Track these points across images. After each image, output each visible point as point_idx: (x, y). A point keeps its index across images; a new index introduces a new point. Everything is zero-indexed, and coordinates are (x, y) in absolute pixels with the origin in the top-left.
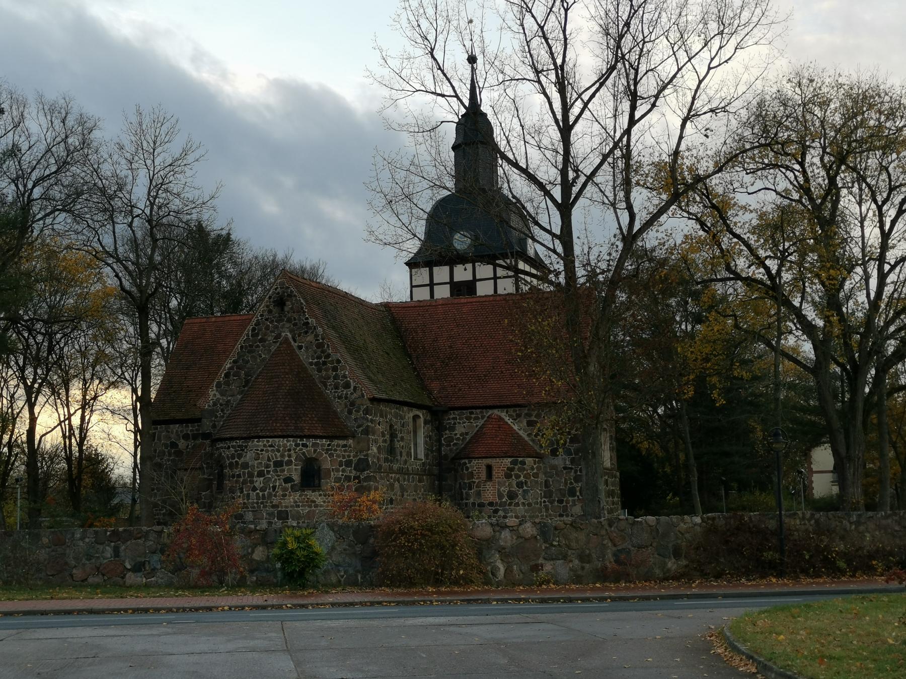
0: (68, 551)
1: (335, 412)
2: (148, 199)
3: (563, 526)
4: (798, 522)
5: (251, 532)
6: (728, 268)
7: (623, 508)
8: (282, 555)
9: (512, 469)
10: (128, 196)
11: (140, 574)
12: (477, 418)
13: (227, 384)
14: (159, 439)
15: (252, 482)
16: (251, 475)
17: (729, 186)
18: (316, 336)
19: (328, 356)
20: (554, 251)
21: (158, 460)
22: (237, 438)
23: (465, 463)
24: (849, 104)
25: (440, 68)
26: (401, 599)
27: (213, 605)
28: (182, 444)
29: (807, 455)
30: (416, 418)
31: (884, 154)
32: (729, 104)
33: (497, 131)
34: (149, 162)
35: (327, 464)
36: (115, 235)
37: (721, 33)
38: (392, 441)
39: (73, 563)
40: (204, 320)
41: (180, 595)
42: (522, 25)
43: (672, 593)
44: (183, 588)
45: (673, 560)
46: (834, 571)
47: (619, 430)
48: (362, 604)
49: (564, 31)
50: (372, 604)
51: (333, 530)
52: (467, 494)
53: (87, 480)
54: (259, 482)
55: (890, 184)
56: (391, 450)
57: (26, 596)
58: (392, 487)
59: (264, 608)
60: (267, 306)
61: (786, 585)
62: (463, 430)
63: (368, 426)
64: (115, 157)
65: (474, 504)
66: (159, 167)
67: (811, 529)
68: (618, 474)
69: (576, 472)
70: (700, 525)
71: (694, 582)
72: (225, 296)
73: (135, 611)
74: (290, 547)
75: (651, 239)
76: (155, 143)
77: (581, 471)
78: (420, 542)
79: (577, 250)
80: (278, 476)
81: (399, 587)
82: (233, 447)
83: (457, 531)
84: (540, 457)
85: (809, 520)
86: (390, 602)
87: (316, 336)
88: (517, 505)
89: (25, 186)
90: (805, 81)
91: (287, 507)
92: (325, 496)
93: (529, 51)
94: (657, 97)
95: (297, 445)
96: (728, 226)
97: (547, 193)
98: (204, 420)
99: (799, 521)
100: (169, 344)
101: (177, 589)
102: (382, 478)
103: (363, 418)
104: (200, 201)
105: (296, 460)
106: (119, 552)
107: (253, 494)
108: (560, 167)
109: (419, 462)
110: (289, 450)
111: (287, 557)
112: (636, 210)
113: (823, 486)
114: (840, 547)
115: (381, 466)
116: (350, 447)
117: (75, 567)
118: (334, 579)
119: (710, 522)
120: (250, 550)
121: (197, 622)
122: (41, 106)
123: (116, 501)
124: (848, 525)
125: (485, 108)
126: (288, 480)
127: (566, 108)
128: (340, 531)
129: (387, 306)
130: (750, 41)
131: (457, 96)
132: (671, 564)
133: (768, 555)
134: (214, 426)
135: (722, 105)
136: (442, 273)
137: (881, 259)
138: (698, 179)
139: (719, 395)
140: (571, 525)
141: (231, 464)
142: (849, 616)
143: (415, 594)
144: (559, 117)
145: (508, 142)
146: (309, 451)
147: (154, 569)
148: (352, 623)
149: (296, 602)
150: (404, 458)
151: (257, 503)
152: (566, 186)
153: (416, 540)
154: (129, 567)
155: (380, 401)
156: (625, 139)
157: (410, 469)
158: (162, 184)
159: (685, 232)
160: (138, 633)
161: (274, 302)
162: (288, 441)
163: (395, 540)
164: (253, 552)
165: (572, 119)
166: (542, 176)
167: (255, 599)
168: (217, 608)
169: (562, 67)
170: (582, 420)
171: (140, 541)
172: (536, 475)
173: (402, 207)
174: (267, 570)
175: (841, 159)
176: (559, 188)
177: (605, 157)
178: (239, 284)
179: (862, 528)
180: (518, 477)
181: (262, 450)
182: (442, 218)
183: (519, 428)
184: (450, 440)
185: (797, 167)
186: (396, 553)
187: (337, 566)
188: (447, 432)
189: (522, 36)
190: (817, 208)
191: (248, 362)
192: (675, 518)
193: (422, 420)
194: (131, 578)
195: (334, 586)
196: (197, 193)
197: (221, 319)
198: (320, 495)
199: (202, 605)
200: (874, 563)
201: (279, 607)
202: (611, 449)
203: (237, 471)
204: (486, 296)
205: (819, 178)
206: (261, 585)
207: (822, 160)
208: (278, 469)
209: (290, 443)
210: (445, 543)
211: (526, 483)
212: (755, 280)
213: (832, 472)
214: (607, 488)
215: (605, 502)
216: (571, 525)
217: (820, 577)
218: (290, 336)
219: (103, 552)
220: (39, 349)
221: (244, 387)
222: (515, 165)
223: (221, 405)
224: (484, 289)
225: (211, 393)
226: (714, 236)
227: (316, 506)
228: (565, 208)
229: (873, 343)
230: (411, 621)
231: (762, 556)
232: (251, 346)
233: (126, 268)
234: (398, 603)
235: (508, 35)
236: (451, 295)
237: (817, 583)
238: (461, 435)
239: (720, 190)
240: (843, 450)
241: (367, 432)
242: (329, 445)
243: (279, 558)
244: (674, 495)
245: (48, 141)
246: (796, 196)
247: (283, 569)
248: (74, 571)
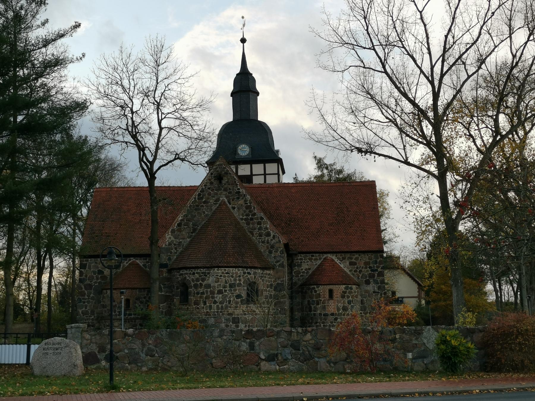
1: (260, 251)
11: (272, 363)
12: (316, 259)
13: (180, 230)
14: (90, 268)
16: (212, 293)
21: (88, 282)
22: (201, 268)
23: (314, 288)
28: (107, 272)
35: (261, 287)
39: (213, 354)
62: (307, 267)
65: (320, 314)
80: (232, 293)
82: (197, 273)
91: (238, 315)
103: (280, 256)
105: (244, 283)
106: (254, 346)
107: (214, 306)
110: (240, 276)
134: (170, 259)
151: (217, 312)
154: (263, 357)
161: (214, 177)
162: (239, 270)
180: (348, 297)
181: (221, 276)
183: (345, 266)
188: (296, 267)
194: (265, 366)
203: (201, 290)
208: (232, 289)
209: (240, 271)
218: (226, 200)
221: (192, 233)
224: (257, 180)
232: (197, 206)
238: (306, 269)
242: (262, 273)
248: (214, 361)
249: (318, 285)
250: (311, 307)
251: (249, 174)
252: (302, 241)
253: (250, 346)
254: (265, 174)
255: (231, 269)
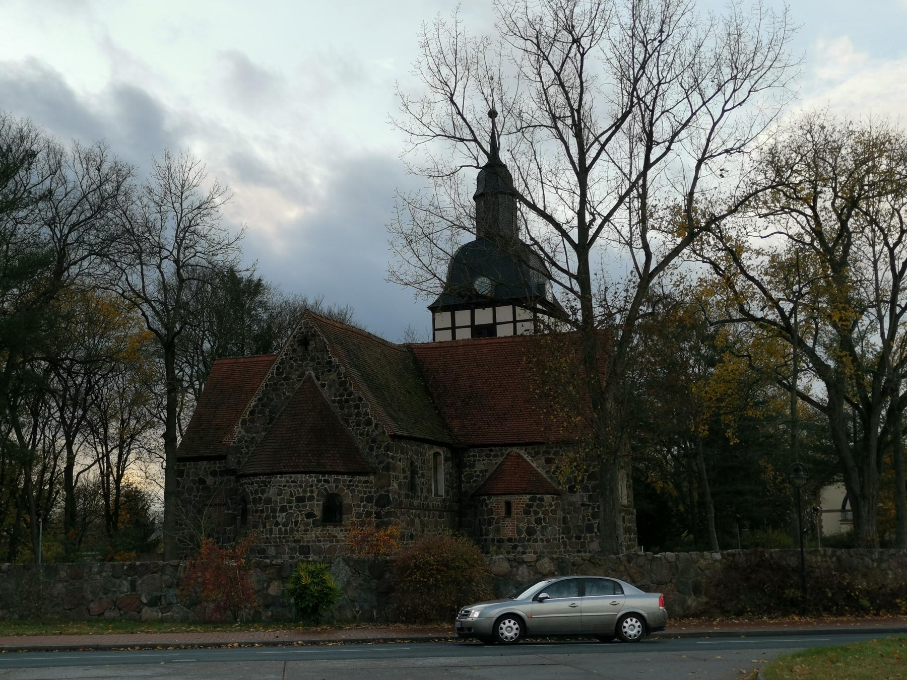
0: (85, 586)
2: (176, 241)
3: (581, 562)
4: (819, 559)
5: (266, 566)
6: (742, 310)
7: (640, 544)
8: (295, 590)
9: (531, 506)
10: (157, 239)
11: (155, 609)
12: (496, 456)
13: (252, 421)
14: (188, 476)
15: (274, 517)
16: (274, 510)
17: (743, 230)
18: (339, 374)
19: (351, 394)
20: (571, 290)
21: (186, 495)
23: (485, 500)
24: (860, 150)
25: (459, 113)
26: (415, 636)
27: (222, 641)
28: (210, 480)
29: (816, 494)
30: (436, 455)
31: (896, 196)
32: (743, 145)
33: (515, 175)
34: (177, 205)
35: (348, 500)
36: (150, 278)
37: (734, 78)
38: (412, 478)
39: (90, 596)
40: (233, 361)
41: (191, 631)
42: (539, 74)
43: (693, 631)
44: (195, 623)
45: (693, 597)
46: (858, 610)
47: (636, 469)
48: (375, 641)
49: (580, 76)
50: (385, 641)
51: (349, 566)
52: (487, 530)
53: (124, 516)
54: (281, 517)
55: (901, 227)
56: (412, 487)
57: (36, 631)
58: (412, 522)
59: (274, 644)
60: (292, 346)
61: (809, 623)
62: (483, 468)
63: (389, 463)
64: (145, 200)
65: (493, 540)
66: (187, 210)
67: (832, 566)
68: (635, 511)
69: (593, 508)
70: (720, 562)
71: (715, 620)
72: (256, 339)
73: (143, 647)
74: (304, 582)
75: (665, 283)
76: (183, 187)
77: (598, 507)
78: (436, 578)
79: (594, 289)
80: (300, 511)
81: (414, 623)
82: (256, 482)
83: (474, 566)
84: (558, 494)
85: (831, 557)
86: (404, 639)
87: (339, 374)
88: (536, 541)
89: (61, 231)
90: (817, 127)
91: (308, 542)
92: (346, 531)
93: (547, 99)
94: (671, 141)
95: (319, 481)
96: (742, 268)
97: (564, 234)
98: (230, 457)
99: (819, 560)
100: (200, 385)
101: (190, 624)
102: (402, 514)
104: (226, 242)
107: (276, 529)
108: (577, 209)
109: (439, 499)
110: (312, 486)
111: (301, 593)
112: (652, 250)
113: (832, 524)
114: (862, 584)
115: (401, 502)
116: (371, 483)
117: (92, 601)
118: (349, 614)
119: (731, 558)
120: (265, 585)
121: (199, 661)
122: (77, 155)
123: (153, 537)
124: (870, 561)
125: (504, 157)
126: (310, 515)
127: (582, 153)
128: (356, 566)
129: (410, 349)
130: (762, 84)
131: (475, 140)
132: (691, 601)
133: (790, 593)
135: (738, 145)
136: (463, 317)
137: (893, 302)
138: (715, 219)
139: (733, 434)
140: (590, 560)
141: (254, 499)
142: (892, 661)
143: (430, 630)
144: (576, 160)
145: (526, 186)
146: (331, 487)
147: (170, 604)
148: (359, 663)
149: (307, 638)
150: (424, 495)
151: (280, 538)
152: (583, 228)
153: (431, 575)
154: (145, 601)
155: (400, 438)
156: (641, 182)
157: (431, 505)
158: (189, 227)
159: (699, 275)
160: (130, 674)
161: (298, 341)
163: (410, 575)
164: (268, 586)
165: (588, 162)
166: (560, 218)
167: (267, 636)
168: (226, 644)
169: (578, 111)
170: (599, 456)
171: (157, 576)
172: (554, 512)
173: (422, 248)
174: (283, 606)
175: (853, 203)
176: (576, 230)
177: (621, 199)
178: (269, 328)
179: (884, 566)
180: (536, 513)
181: (285, 486)
182: (464, 263)
184: (470, 476)
185: (809, 212)
186: (411, 588)
187: (352, 601)
189: (539, 85)
190: (829, 251)
191: (272, 400)
192: (694, 554)
193: (442, 457)
194: (147, 612)
195: (349, 622)
196: (223, 234)
197: (250, 360)
198: (341, 530)
199: (211, 641)
200: (898, 601)
201: (290, 644)
202: (628, 487)
204: (505, 337)
205: (830, 223)
206: (276, 621)
207: (833, 204)
208: (301, 505)
209: (312, 479)
210: (461, 579)
211: (544, 519)
212: (769, 322)
213: (840, 511)
214: (625, 524)
215: (623, 537)
216: (590, 560)
217: (842, 615)
218: (313, 374)
219: (120, 586)
220: (77, 391)
221: (268, 424)
222: (533, 207)
223: (246, 442)
224: (504, 331)
225: (236, 430)
226: (729, 279)
227: (338, 541)
228: (583, 248)
229: (887, 381)
230: (420, 662)
231: (784, 593)
232: (275, 384)
233: (153, 308)
234: (412, 640)
235: (524, 84)
236: (472, 336)
237: (842, 622)
239: (733, 234)
240: (857, 489)
241: (387, 468)
242: (350, 481)
243: (293, 592)
244: (689, 533)
245: (84, 187)
246: (808, 239)
247: (296, 604)
249: (490, 495)
250: (481, 529)
251: (492, 322)
252: (480, 428)
253: (131, 585)
254: (515, 322)
255: (299, 476)
